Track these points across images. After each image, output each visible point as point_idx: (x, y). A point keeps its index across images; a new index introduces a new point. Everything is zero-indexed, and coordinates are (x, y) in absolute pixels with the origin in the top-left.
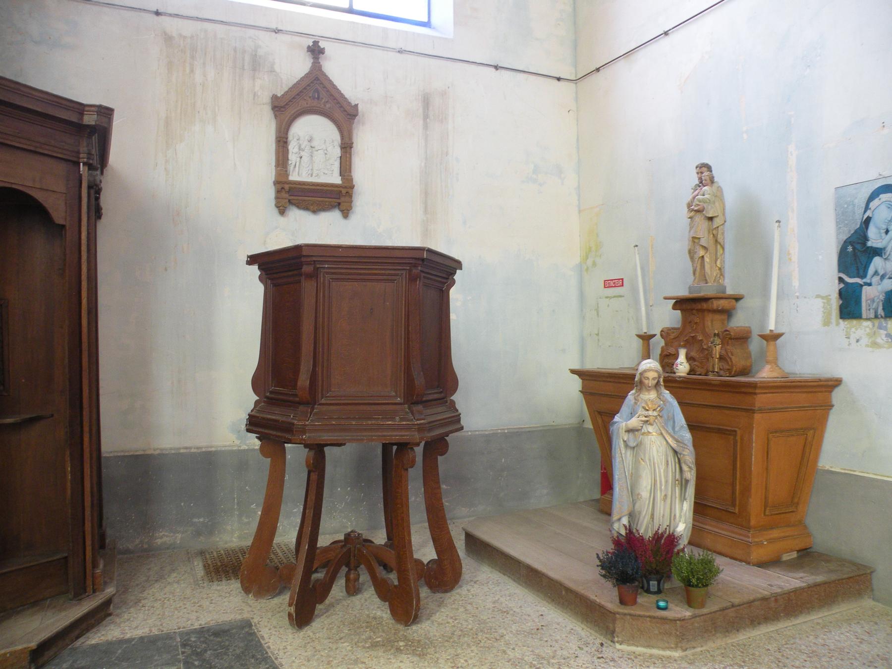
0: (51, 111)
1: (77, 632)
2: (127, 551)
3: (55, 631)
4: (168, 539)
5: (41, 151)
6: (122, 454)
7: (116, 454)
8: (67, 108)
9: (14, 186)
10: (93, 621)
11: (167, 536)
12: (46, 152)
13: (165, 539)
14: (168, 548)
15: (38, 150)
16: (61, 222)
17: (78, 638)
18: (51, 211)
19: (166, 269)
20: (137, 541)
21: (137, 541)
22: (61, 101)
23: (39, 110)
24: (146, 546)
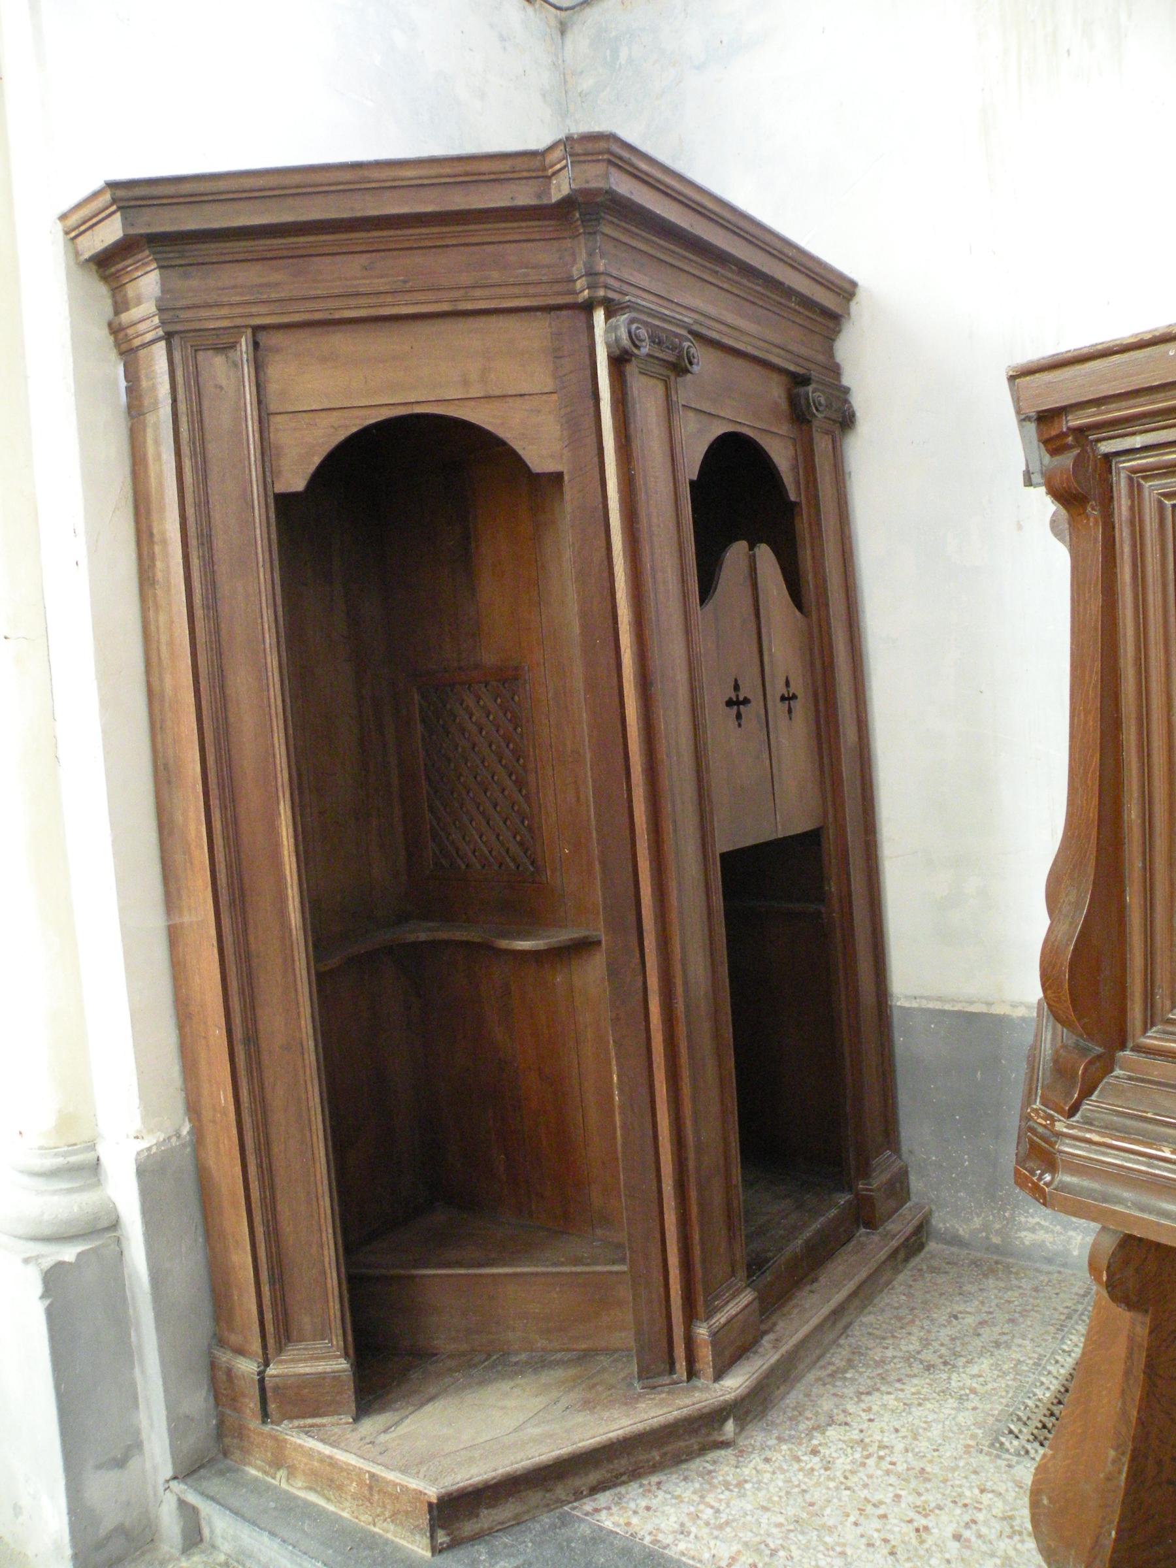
0: (459, 201)
1: (594, 1477)
2: (955, 1240)
3: (501, 1471)
4: (1048, 1238)
5: (469, 306)
6: (937, 1005)
7: (925, 1004)
8: (497, 180)
9: (418, 410)
10: (656, 1455)
11: (1047, 1230)
12: (483, 305)
13: (1041, 1236)
14: (1049, 1261)
15: (463, 306)
16: (549, 466)
17: (595, 1490)
18: (517, 446)
19: (1020, 527)
20: (977, 1222)
21: (977, 1222)
22: (485, 167)
23: (430, 208)
24: (996, 1240)
